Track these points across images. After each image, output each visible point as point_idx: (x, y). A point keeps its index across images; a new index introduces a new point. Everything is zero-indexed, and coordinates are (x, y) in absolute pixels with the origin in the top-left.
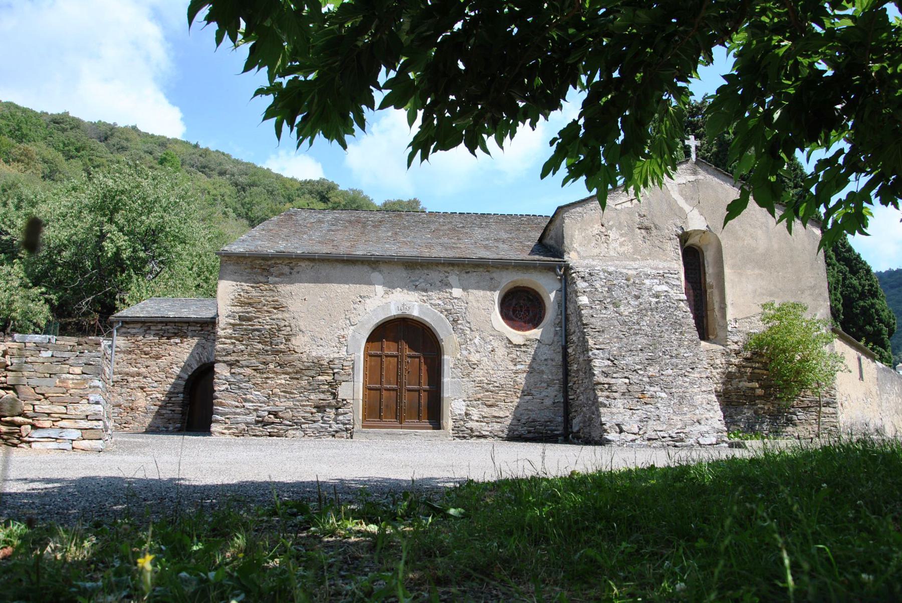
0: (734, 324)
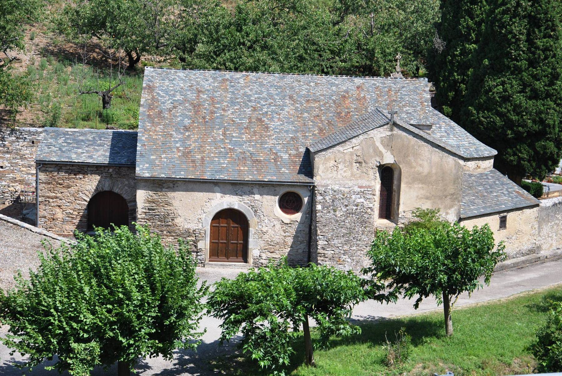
0: (403, 214)
